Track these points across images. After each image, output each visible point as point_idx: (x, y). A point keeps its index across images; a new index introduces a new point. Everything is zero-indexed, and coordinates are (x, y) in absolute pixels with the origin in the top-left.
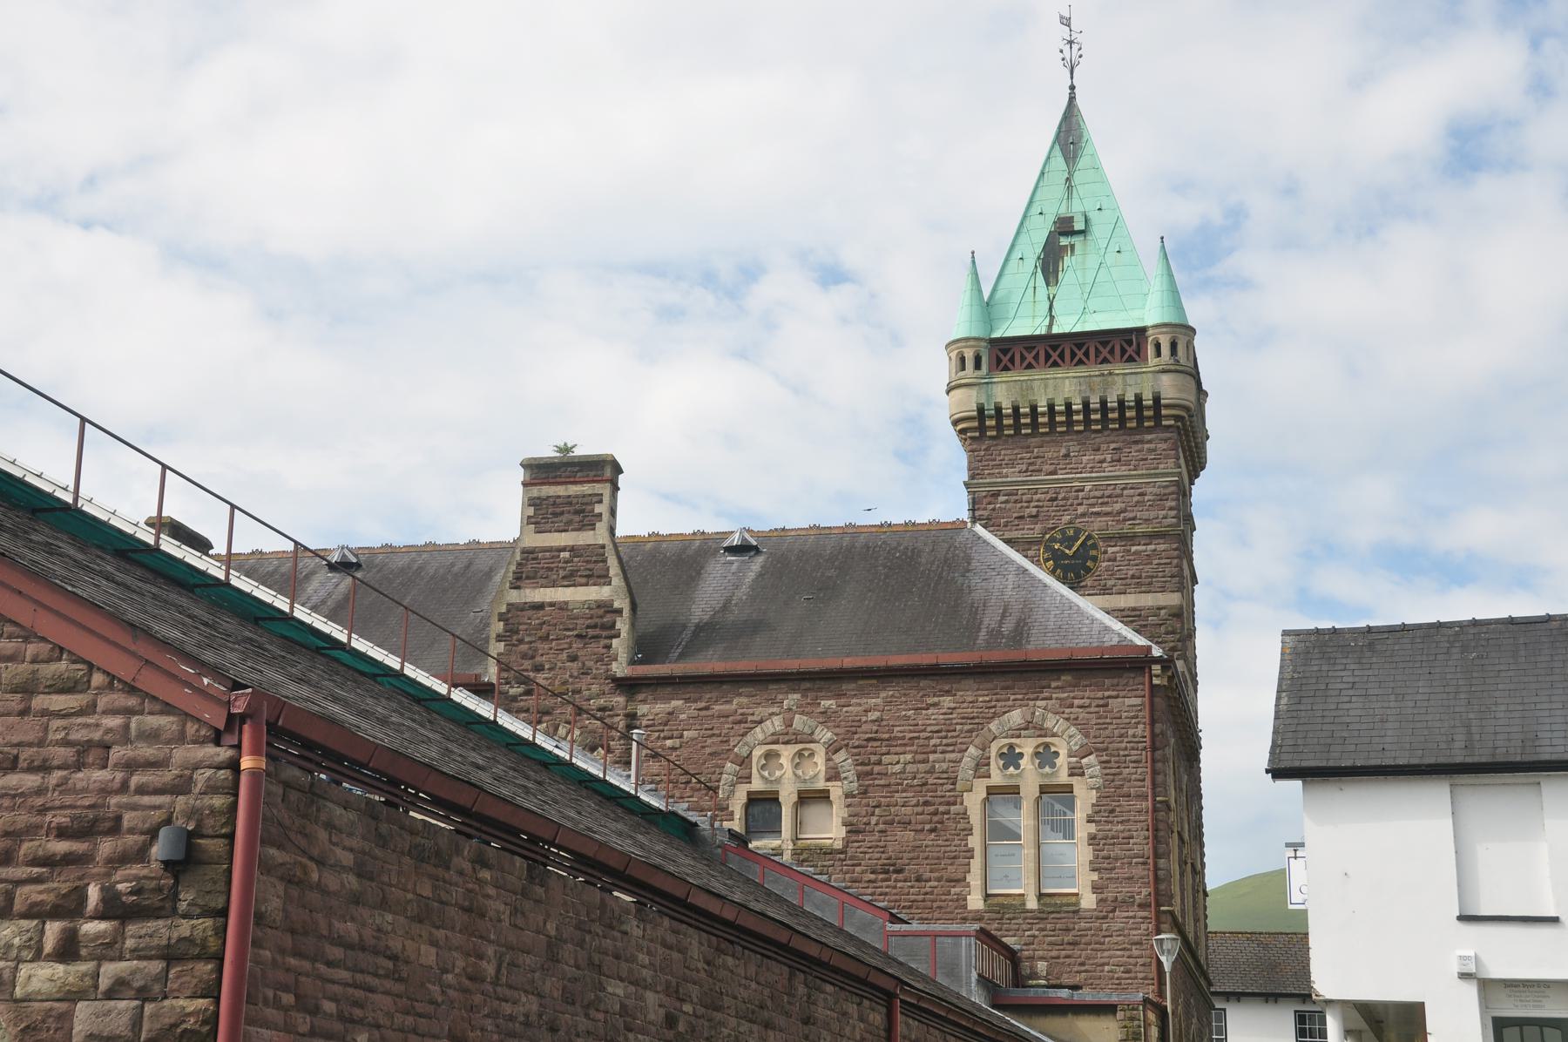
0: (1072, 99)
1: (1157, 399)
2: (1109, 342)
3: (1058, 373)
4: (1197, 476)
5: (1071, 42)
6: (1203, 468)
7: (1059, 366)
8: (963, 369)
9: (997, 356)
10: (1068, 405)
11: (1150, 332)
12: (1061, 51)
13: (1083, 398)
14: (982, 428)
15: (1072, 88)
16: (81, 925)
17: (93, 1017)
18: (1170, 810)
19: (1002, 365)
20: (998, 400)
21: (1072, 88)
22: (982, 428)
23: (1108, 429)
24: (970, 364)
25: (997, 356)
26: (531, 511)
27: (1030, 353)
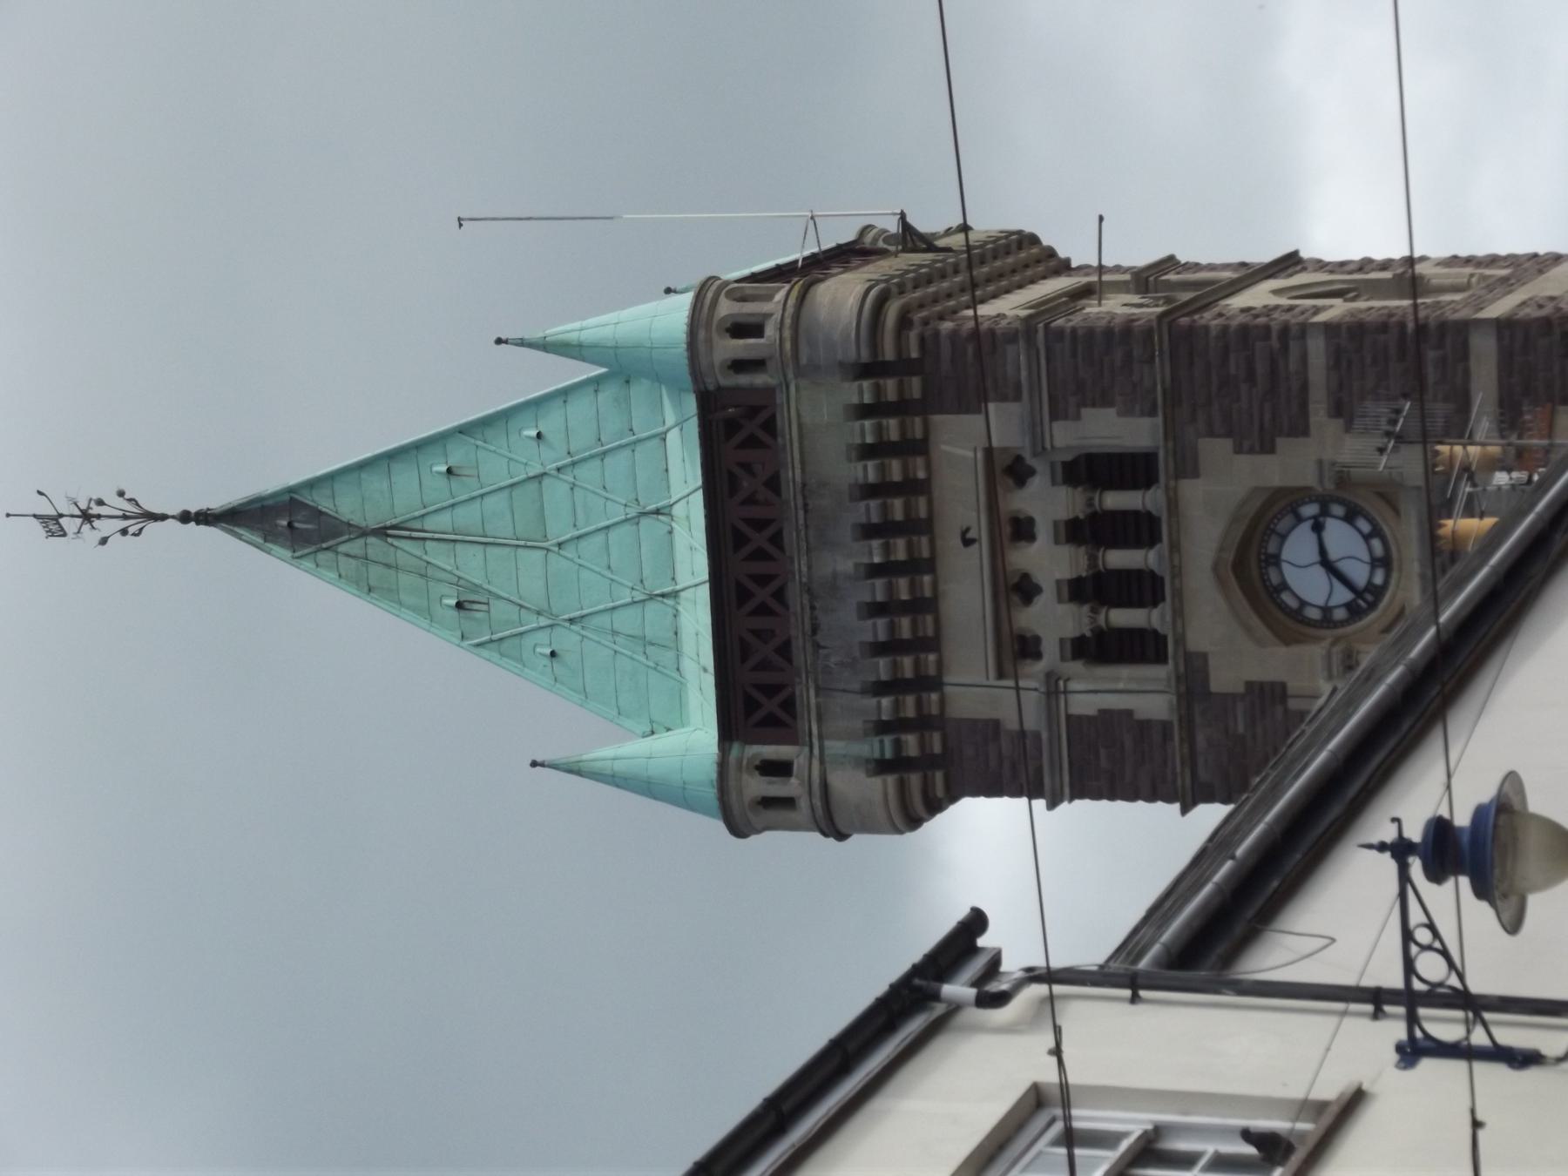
0: (205, 518)
2: (742, 640)
4: (1051, 253)
6: (1033, 240)
7: (773, 417)
8: (788, 803)
10: (863, 411)
12: (104, 541)
13: (853, 499)
14: (926, 763)
15: (185, 517)
16: (1272, 584)
19: (761, 434)
21: (185, 517)
22: (926, 763)
23: (920, 360)
24: (775, 788)
27: (759, 705)
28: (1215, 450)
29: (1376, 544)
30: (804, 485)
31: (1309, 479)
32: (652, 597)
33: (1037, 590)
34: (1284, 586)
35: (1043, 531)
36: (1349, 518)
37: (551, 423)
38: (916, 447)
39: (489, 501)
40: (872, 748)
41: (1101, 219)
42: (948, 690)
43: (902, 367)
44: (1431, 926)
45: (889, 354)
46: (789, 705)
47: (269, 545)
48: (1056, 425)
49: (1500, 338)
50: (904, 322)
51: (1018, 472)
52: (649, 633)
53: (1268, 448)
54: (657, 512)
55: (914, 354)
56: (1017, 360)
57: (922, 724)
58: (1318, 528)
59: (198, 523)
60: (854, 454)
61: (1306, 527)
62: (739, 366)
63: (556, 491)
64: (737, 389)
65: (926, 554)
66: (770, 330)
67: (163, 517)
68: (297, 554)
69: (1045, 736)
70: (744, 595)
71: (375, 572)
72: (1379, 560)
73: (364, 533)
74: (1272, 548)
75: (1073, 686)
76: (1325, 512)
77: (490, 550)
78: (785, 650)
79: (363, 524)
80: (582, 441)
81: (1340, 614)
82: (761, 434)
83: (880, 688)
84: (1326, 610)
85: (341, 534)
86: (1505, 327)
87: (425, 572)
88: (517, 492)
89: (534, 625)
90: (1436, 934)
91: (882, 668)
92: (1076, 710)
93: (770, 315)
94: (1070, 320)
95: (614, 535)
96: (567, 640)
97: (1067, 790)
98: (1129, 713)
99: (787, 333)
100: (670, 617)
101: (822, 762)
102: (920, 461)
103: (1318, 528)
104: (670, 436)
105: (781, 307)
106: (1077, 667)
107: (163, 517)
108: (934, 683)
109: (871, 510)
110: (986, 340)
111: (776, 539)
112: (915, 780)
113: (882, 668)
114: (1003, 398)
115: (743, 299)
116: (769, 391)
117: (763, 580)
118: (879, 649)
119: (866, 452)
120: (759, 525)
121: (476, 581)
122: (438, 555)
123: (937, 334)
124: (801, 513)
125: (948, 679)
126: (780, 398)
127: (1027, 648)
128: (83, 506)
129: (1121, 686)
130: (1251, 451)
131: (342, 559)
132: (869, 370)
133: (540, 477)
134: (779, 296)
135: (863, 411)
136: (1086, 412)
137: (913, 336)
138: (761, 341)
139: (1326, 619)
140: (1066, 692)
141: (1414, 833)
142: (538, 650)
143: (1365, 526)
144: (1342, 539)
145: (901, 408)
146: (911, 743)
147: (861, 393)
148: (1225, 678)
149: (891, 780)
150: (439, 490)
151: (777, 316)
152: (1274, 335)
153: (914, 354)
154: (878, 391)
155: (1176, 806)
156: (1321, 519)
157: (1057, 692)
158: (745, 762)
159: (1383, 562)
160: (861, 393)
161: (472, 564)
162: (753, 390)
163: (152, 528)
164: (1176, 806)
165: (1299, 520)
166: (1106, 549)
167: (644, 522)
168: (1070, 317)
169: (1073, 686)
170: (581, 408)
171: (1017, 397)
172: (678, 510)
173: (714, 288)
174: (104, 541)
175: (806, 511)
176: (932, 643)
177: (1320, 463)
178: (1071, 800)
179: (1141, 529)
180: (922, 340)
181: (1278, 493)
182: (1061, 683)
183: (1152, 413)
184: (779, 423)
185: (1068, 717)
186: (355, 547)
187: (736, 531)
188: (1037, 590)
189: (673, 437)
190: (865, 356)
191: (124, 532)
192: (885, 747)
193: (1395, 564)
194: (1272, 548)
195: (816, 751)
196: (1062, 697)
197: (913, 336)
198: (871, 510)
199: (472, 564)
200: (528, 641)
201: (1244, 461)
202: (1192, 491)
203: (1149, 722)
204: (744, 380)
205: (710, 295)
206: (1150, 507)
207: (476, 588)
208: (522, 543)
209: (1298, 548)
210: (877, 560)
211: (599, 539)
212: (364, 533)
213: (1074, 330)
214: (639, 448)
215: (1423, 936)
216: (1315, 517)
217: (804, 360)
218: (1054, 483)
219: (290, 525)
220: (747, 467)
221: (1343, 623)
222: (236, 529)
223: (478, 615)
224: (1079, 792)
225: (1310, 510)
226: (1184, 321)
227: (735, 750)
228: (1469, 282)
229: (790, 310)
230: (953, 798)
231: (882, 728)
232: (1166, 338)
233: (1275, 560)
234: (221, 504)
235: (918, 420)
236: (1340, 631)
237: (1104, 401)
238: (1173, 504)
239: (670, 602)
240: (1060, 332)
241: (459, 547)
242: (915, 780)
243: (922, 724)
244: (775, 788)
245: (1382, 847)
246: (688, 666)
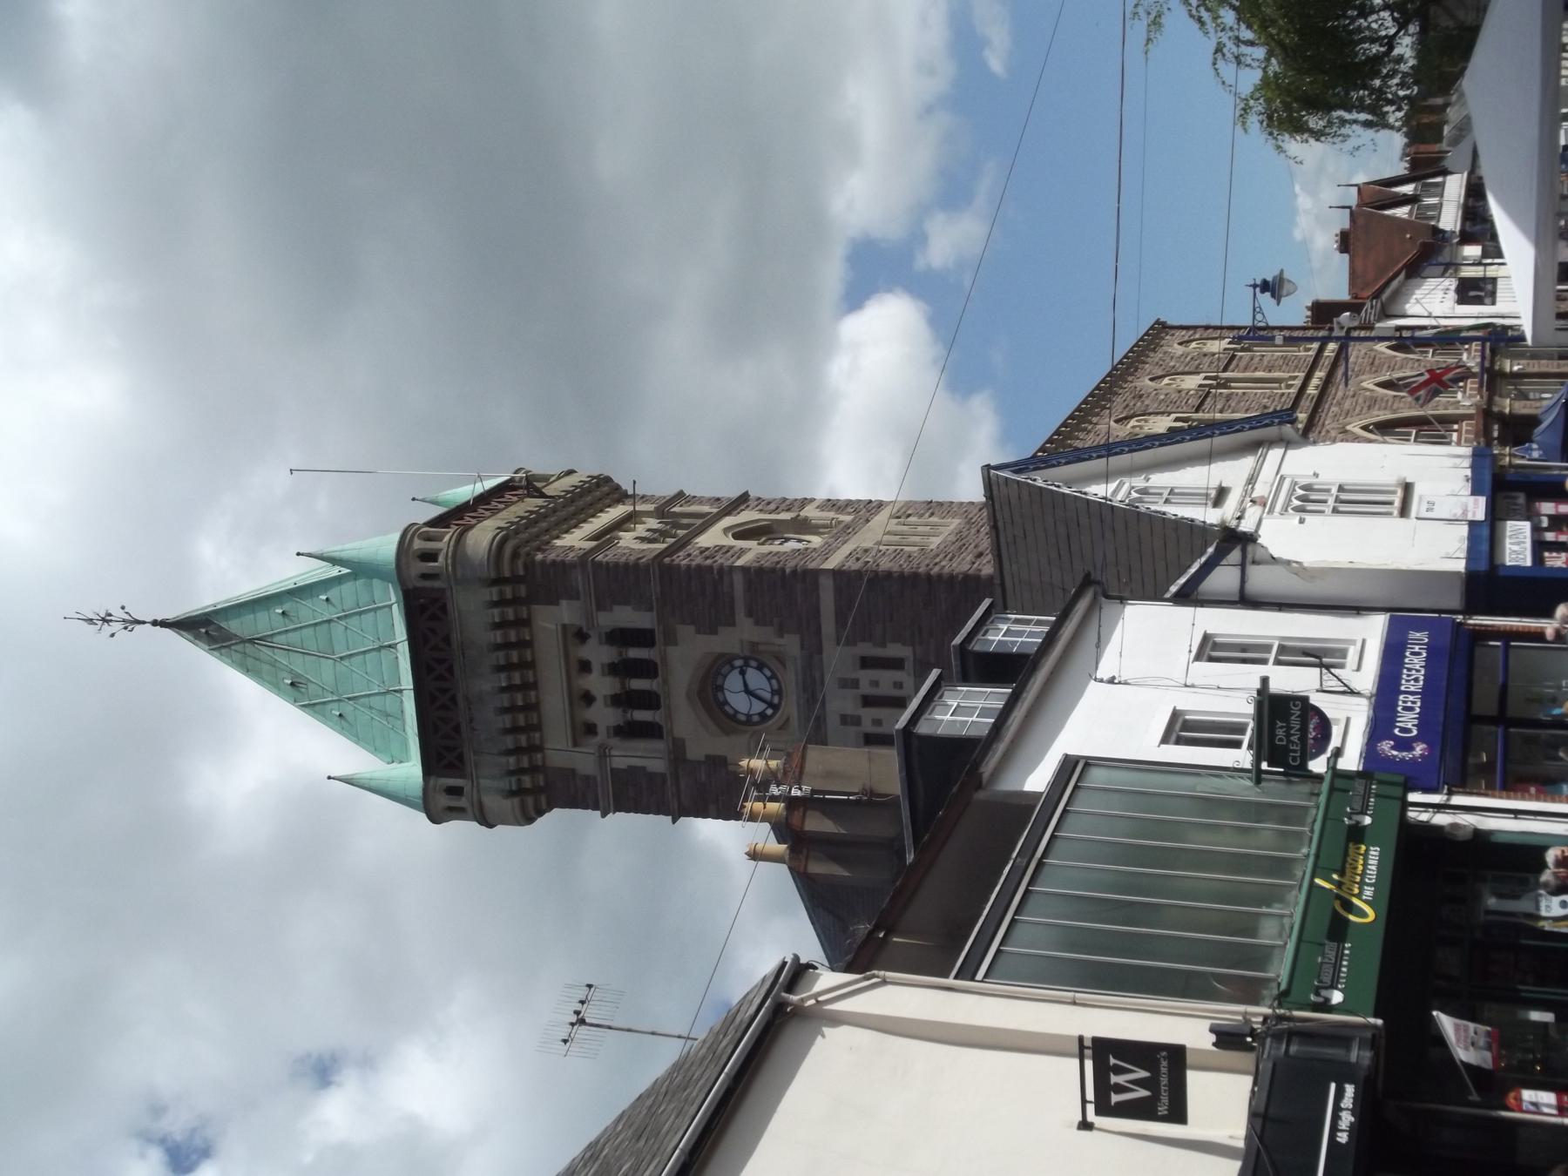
0: (163, 624)
6: (608, 480)
10: (495, 604)
15: (155, 623)
21: (155, 623)
22: (535, 791)
24: (454, 802)
28: (686, 632)
29: (774, 682)
30: (462, 643)
31: (736, 650)
32: (388, 692)
34: (726, 702)
35: (596, 667)
36: (760, 668)
37: (333, 593)
38: (526, 623)
39: (305, 631)
40: (504, 784)
41: (634, 482)
42: (548, 752)
43: (514, 580)
45: (507, 574)
46: (461, 757)
47: (197, 641)
48: (599, 613)
49: (835, 579)
50: (515, 555)
51: (582, 636)
52: (388, 710)
53: (713, 632)
54: (390, 646)
55: (521, 573)
56: (578, 579)
57: (533, 770)
58: (743, 673)
59: (161, 627)
61: (736, 672)
62: (425, 576)
63: (338, 629)
64: (424, 589)
65: (531, 680)
66: (441, 558)
67: (144, 623)
68: (211, 647)
69: (599, 779)
71: (250, 661)
72: (776, 691)
73: (244, 641)
74: (719, 682)
75: (614, 753)
76: (747, 665)
77: (307, 657)
78: (457, 729)
79: (242, 636)
80: (349, 603)
81: (756, 718)
83: (509, 753)
84: (749, 716)
85: (231, 639)
86: (837, 574)
87: (274, 664)
88: (318, 628)
89: (371, 647)
91: (509, 742)
92: (615, 766)
93: (441, 550)
94: (607, 556)
95: (368, 656)
96: (348, 708)
97: (612, 808)
98: (643, 769)
99: (449, 561)
100: (398, 703)
101: (478, 791)
102: (526, 630)
103: (743, 673)
104: (393, 606)
105: (446, 546)
106: (614, 741)
107: (144, 623)
108: (540, 749)
109: (500, 657)
110: (561, 568)
111: (450, 670)
112: (530, 801)
113: (509, 742)
114: (570, 598)
115: (429, 539)
116: (443, 591)
118: (507, 731)
119: (497, 626)
120: (441, 661)
121: (300, 672)
122: (281, 658)
123: (533, 561)
124: (462, 658)
125: (548, 745)
126: (448, 594)
127: (591, 729)
128: (103, 615)
129: (639, 754)
130: (705, 633)
131: (233, 652)
132: (498, 581)
133: (329, 621)
134: (447, 538)
135: (495, 604)
136: (616, 608)
137: (520, 563)
138: (436, 564)
139: (749, 721)
140: (610, 756)
141: (1258, 282)
142: (333, 712)
143: (768, 673)
144: (756, 679)
145: (515, 601)
146: (527, 781)
147: (491, 594)
148: (695, 752)
149: (516, 800)
150: (279, 624)
151: (445, 551)
152: (715, 572)
153: (521, 573)
154: (501, 593)
155: (670, 818)
156: (744, 668)
157: (605, 756)
158: (437, 788)
159: (778, 692)
160: (491, 594)
161: (299, 664)
162: (433, 589)
163: (138, 627)
164: (670, 818)
165: (733, 668)
166: (630, 678)
167: (383, 651)
168: (607, 553)
169: (614, 753)
170: (347, 588)
171: (578, 598)
172: (399, 646)
173: (415, 527)
174: (112, 635)
175: (464, 658)
176: (538, 727)
177: (742, 641)
178: (614, 813)
179: (647, 669)
180: (526, 567)
181: (721, 655)
182: (607, 751)
183: (651, 609)
184: (448, 607)
185: (612, 770)
186: (239, 647)
189: (395, 607)
190: (493, 575)
191: (126, 628)
192: (512, 783)
193: (784, 694)
194: (719, 682)
195: (475, 784)
196: (608, 759)
197: (520, 563)
198: (500, 657)
199: (299, 664)
200: (329, 707)
201: (701, 637)
202: (673, 652)
203: (655, 774)
204: (428, 584)
205: (409, 537)
206: (652, 657)
207: (300, 676)
208: (321, 655)
209: (733, 682)
210: (504, 685)
211: (360, 658)
212: (244, 641)
213: (607, 563)
214: (378, 612)
215: (1258, 310)
216: (741, 667)
217: (459, 574)
218: (601, 643)
219: (207, 632)
222: (181, 632)
223: (303, 690)
224: (618, 809)
225: (738, 663)
226: (667, 560)
227: (432, 782)
228: (831, 523)
229: (451, 548)
230: (550, 809)
231: (511, 773)
232: (657, 570)
233: (721, 688)
234: (175, 615)
235: (524, 609)
236: (756, 728)
237: (625, 602)
238: (664, 658)
239: (398, 695)
240: (600, 563)
241: (290, 653)
242: (530, 801)
243: (533, 770)
244: (454, 802)
246: (408, 729)
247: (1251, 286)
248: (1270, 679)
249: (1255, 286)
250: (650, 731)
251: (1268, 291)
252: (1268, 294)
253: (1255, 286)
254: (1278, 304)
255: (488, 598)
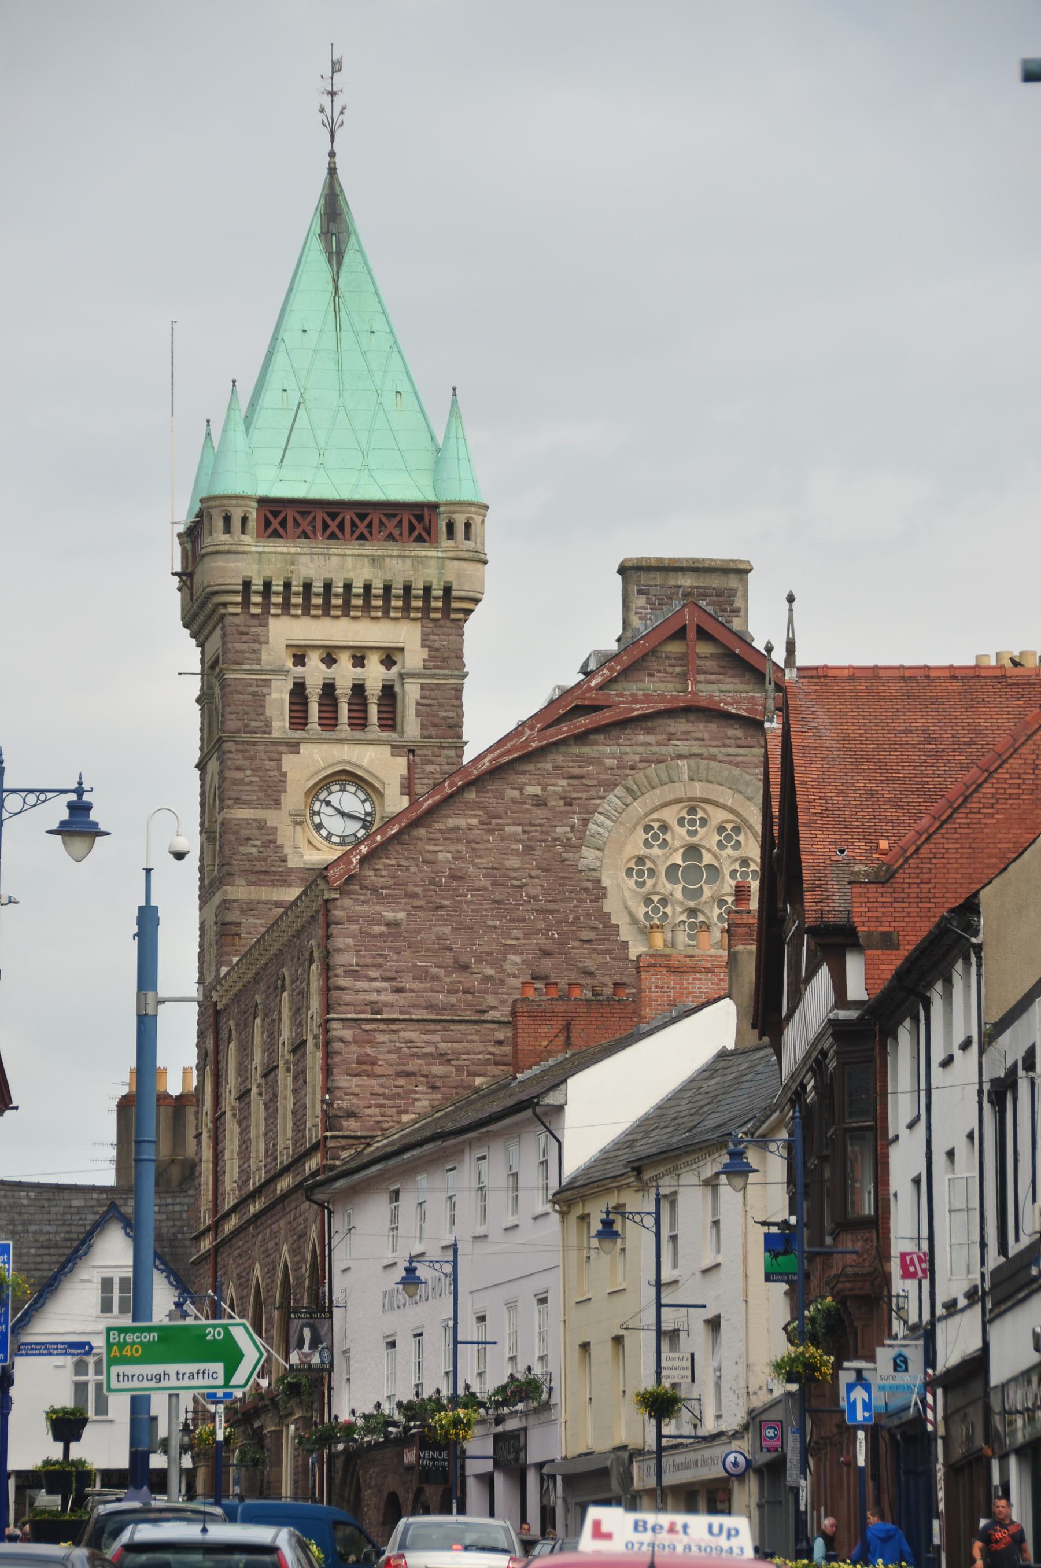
0: (332, 171)
1: (447, 590)
3: (334, 548)
5: (332, 94)
9: (266, 517)
11: (442, 509)
17: (255, 824)
18: (533, 979)
20: (449, 579)
21: (332, 154)
23: (428, 618)
25: (266, 517)
26: (738, 603)
33: (329, 667)
44: (46, 800)
51: (388, 661)
57: (266, 605)
60: (348, 582)
70: (333, 516)
82: (416, 533)
90: (43, 802)
117: (341, 526)
141: (86, 797)
148: (288, 762)
176: (386, 609)
179: (359, 722)
187: (366, 515)
188: (329, 667)
215: (42, 797)
220: (400, 524)
221: (312, 821)
242: (239, 599)
245: (80, 783)
247: (80, 783)
248: (626, 1339)
249: (80, 791)
250: (299, 718)
251: (71, 815)
252: (65, 815)
253: (80, 791)
254: (50, 832)
255: (434, 587)
